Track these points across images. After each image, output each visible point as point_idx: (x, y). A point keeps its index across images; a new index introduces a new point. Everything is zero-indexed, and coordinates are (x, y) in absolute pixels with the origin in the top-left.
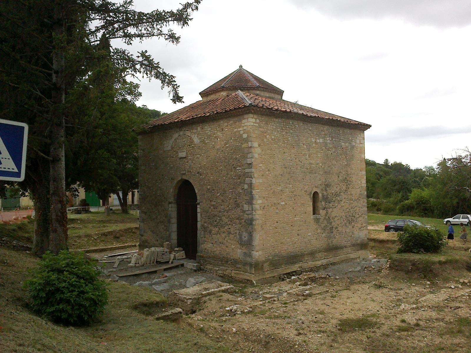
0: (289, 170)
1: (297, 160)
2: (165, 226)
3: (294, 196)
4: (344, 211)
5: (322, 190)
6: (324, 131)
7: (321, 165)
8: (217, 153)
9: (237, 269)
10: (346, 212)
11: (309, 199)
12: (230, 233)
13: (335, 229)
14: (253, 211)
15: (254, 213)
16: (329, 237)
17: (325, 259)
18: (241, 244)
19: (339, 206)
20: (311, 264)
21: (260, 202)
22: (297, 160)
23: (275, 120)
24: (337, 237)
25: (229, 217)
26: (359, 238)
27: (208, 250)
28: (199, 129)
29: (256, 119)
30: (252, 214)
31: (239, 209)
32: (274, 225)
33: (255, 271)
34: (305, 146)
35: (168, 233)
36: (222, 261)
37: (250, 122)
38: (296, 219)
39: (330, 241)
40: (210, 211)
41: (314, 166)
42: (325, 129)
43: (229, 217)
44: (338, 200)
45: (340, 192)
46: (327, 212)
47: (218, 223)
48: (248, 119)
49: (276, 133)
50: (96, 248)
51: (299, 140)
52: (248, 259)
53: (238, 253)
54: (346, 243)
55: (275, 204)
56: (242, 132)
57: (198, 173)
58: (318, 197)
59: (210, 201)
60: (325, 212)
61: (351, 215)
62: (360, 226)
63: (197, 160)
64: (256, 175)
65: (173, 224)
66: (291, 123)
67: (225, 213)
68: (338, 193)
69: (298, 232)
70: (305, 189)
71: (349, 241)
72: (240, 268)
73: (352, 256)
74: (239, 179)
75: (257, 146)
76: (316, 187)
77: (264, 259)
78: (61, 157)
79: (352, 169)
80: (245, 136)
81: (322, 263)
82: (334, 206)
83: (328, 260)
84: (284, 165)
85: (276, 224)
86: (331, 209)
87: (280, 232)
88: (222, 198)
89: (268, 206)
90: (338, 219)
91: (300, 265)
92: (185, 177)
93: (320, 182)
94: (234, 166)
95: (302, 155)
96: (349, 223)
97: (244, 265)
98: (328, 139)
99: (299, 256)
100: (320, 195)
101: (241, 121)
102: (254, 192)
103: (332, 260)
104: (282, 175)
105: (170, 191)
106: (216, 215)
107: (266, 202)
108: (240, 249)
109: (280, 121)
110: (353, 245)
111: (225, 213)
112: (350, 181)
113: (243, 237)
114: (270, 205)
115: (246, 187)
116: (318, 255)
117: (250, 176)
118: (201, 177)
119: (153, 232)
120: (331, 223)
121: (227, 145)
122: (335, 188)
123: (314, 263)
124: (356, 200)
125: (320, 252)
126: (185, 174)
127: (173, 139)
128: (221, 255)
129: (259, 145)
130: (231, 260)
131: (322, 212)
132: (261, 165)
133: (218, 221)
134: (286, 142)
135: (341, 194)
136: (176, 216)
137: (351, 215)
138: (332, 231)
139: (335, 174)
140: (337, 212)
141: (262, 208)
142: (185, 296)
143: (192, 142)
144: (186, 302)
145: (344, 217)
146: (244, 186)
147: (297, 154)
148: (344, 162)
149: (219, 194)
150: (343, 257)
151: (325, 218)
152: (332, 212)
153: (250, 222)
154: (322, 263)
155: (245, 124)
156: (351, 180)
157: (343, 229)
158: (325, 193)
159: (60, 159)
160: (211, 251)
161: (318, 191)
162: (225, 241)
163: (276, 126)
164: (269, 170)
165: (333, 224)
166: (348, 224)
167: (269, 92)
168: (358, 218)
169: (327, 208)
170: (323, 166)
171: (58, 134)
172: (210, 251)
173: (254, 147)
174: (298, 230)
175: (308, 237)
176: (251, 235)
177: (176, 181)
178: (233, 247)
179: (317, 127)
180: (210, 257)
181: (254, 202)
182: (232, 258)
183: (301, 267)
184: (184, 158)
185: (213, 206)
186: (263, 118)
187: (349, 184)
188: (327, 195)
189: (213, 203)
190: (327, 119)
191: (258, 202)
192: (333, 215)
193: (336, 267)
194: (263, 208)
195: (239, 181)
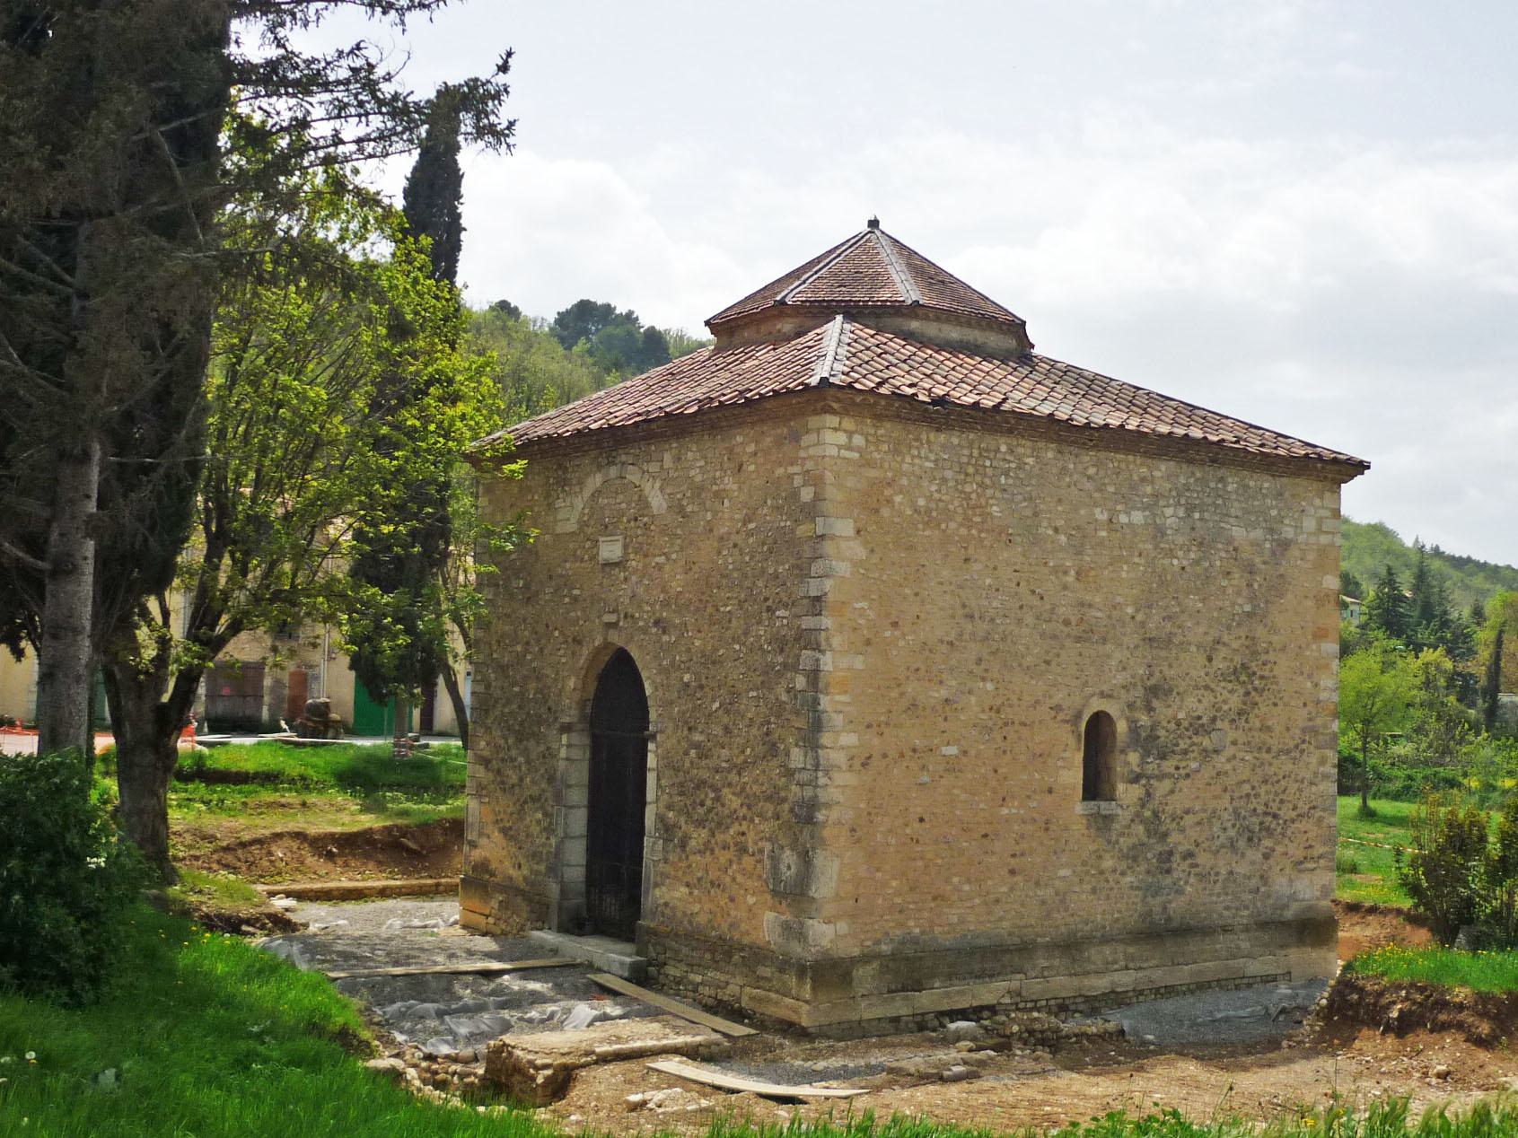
0: (982, 627)
1: (1023, 588)
2: (546, 814)
3: (1000, 723)
4: (1225, 790)
5: (1131, 706)
6: (1152, 483)
7: (1130, 610)
8: (719, 553)
9: (758, 981)
10: (1236, 795)
11: (1072, 742)
12: (743, 850)
13: (1184, 858)
14: (820, 774)
15: (822, 781)
16: (1153, 890)
17: (1127, 968)
18: (775, 893)
19: (1208, 772)
20: (1062, 984)
21: (849, 739)
22: (1023, 588)
23: (932, 436)
24: (1189, 889)
25: (743, 789)
26: (1293, 897)
27: (674, 909)
28: (668, 459)
29: (850, 434)
30: (813, 784)
31: (775, 762)
32: (908, 831)
33: (814, 989)
34: (1063, 538)
35: (553, 841)
36: (713, 952)
37: (833, 439)
38: (1005, 811)
39: (1159, 900)
40: (687, 764)
41: (1099, 614)
42: (1157, 474)
43: (743, 789)
44: (1205, 750)
45: (1214, 720)
46: (1148, 794)
47: (710, 810)
48: (818, 431)
49: (934, 488)
50: (317, 886)
51: (1036, 514)
52: (796, 949)
53: (766, 925)
54: (1226, 913)
55: (914, 750)
56: (798, 481)
57: (657, 623)
58: (1114, 733)
59: (690, 729)
60: (1136, 791)
61: (1261, 809)
62: (1299, 854)
63: (656, 574)
64: (835, 642)
65: (572, 807)
66: (1003, 448)
67: (733, 777)
68: (1204, 720)
69: (1012, 861)
70: (1055, 701)
71: (1246, 908)
72: (766, 979)
73: (1255, 967)
74: (782, 651)
75: (852, 533)
76: (1102, 695)
77: (856, 952)
78: (81, 562)
79: (1273, 630)
80: (807, 495)
81: (1112, 983)
82: (1182, 772)
83: (1140, 974)
84: (964, 606)
85: (917, 825)
86: (1167, 784)
87: (929, 856)
88: (725, 720)
89: (885, 756)
90: (1199, 823)
91: (1015, 984)
92: (616, 639)
93: (1121, 678)
94: (769, 603)
95: (1046, 571)
96: (1250, 840)
97: (781, 970)
98: (1169, 512)
99: (1009, 951)
100: (1122, 727)
101: (795, 438)
102: (825, 702)
103: (1160, 976)
104: (951, 644)
105: (571, 688)
106: (704, 782)
107: (876, 741)
108: (772, 909)
109: (955, 441)
110: (1263, 925)
111: (733, 777)
112: (1262, 677)
113: (783, 868)
114: (893, 754)
115: (800, 682)
116: (1096, 955)
117: (809, 640)
118: (665, 638)
119: (505, 831)
120: (1165, 835)
121: (752, 526)
122: (1191, 701)
123: (1075, 981)
124: (1288, 752)
125: (1106, 940)
126: (614, 625)
127: (587, 493)
128: (713, 928)
129: (858, 532)
130: (742, 950)
131: (1127, 793)
132: (865, 604)
133: (709, 803)
134: (978, 519)
135: (1219, 724)
136: (585, 780)
137: (1261, 809)
138: (1166, 866)
139: (1193, 649)
140: (1193, 796)
141: (857, 763)
142: (530, 1057)
143: (643, 503)
144: (533, 1079)
145: (1226, 816)
146: (793, 680)
147: (1026, 567)
148: (1240, 601)
149: (717, 705)
150: (1210, 968)
151: (1138, 815)
152: (1172, 792)
153: (807, 814)
154: (1112, 983)
155: (811, 451)
156: (1267, 674)
157: (1221, 863)
158: (1144, 719)
159: (75, 567)
160: (684, 914)
161: (1113, 709)
162: (728, 880)
163: (936, 461)
164: (895, 625)
165: (1174, 838)
166: (1242, 844)
167: (960, 324)
168: (1293, 821)
169: (1148, 778)
170: (1139, 617)
171: (77, 489)
172: (679, 914)
173: (833, 537)
174: (1013, 856)
175: (1057, 883)
176: (806, 859)
177: (585, 652)
178: (751, 900)
179: (1123, 466)
180: (676, 935)
181: (826, 739)
182: (746, 941)
183: (1019, 995)
184: (616, 564)
185: (697, 746)
186: (881, 432)
187: (1255, 689)
188: (1153, 728)
189: (697, 737)
190: (1161, 436)
191: (841, 741)
192: (1177, 803)
193: (1168, 1006)
194: (863, 765)
195: (780, 659)
